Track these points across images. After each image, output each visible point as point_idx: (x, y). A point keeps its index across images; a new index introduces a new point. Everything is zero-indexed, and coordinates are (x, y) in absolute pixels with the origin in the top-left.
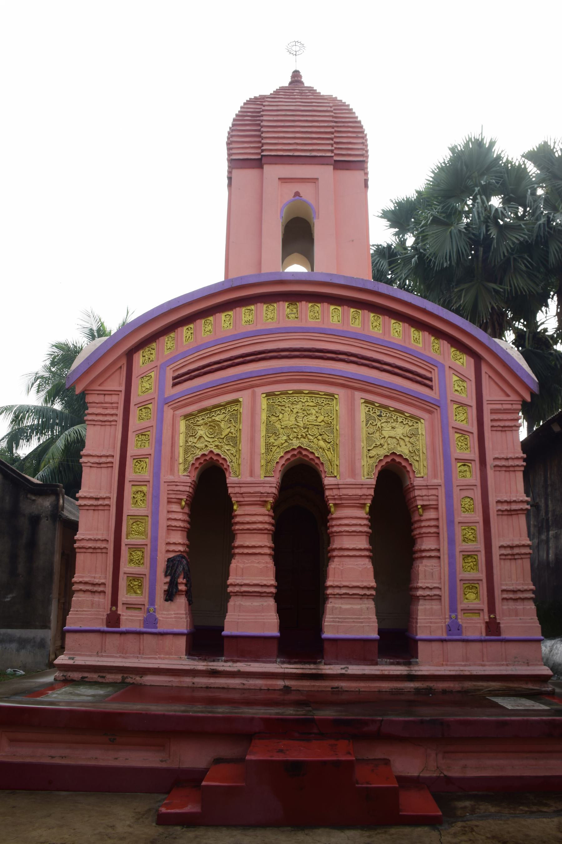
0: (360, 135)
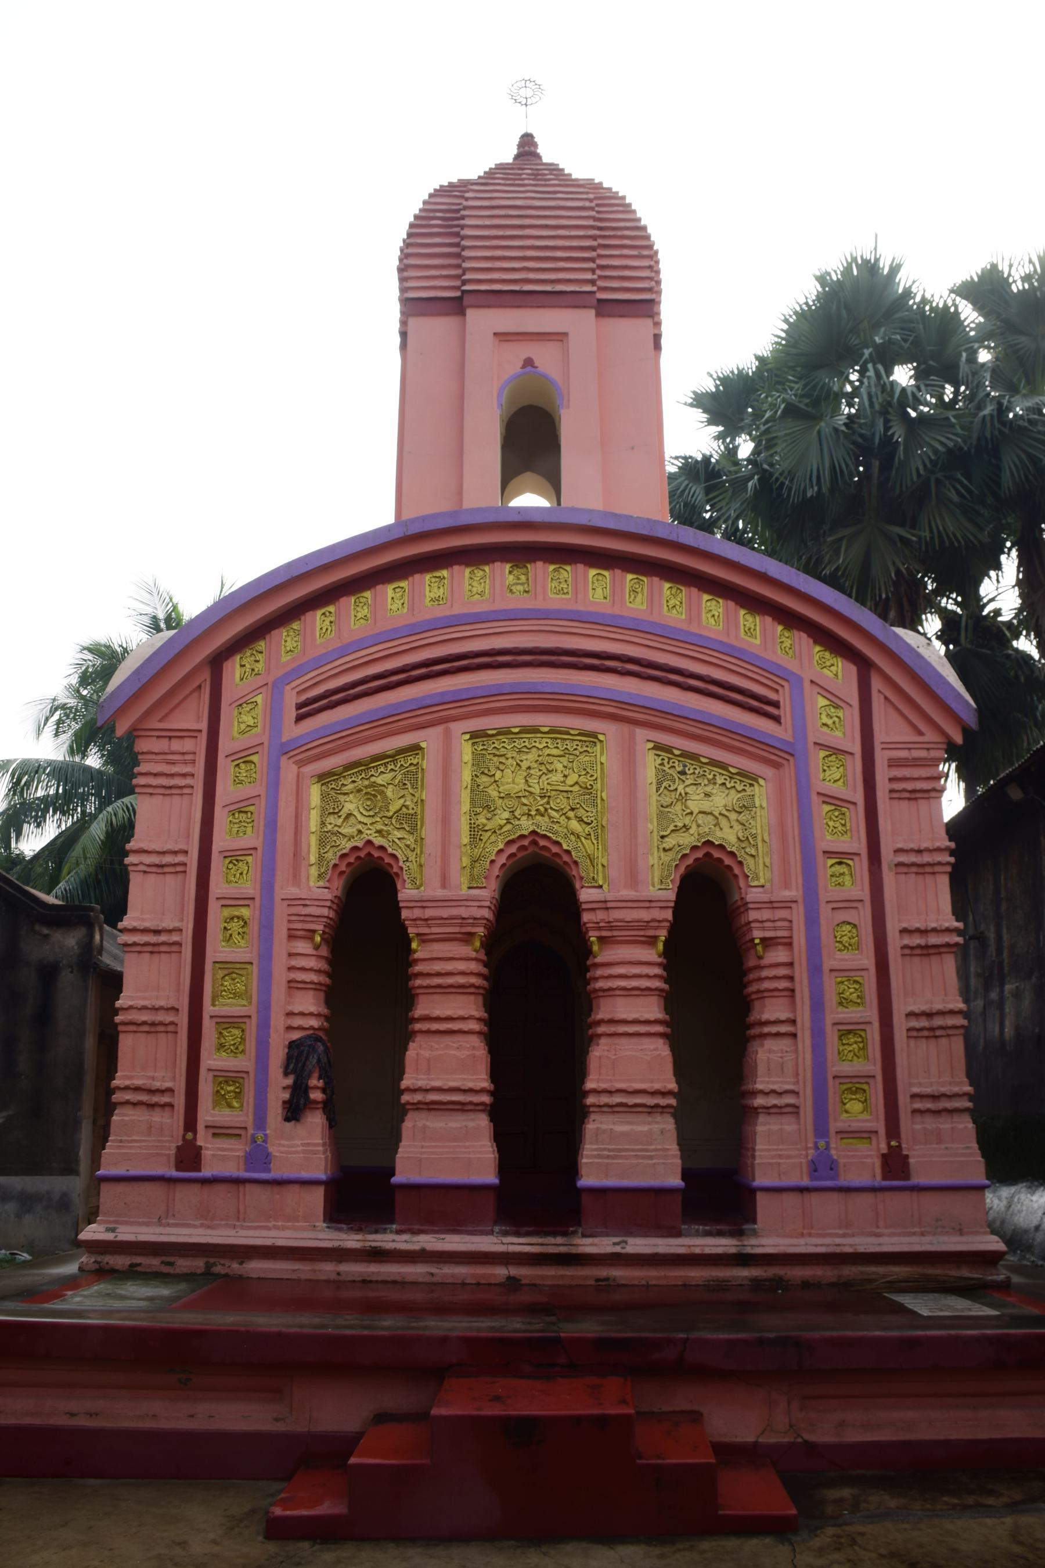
0: (645, 252)
